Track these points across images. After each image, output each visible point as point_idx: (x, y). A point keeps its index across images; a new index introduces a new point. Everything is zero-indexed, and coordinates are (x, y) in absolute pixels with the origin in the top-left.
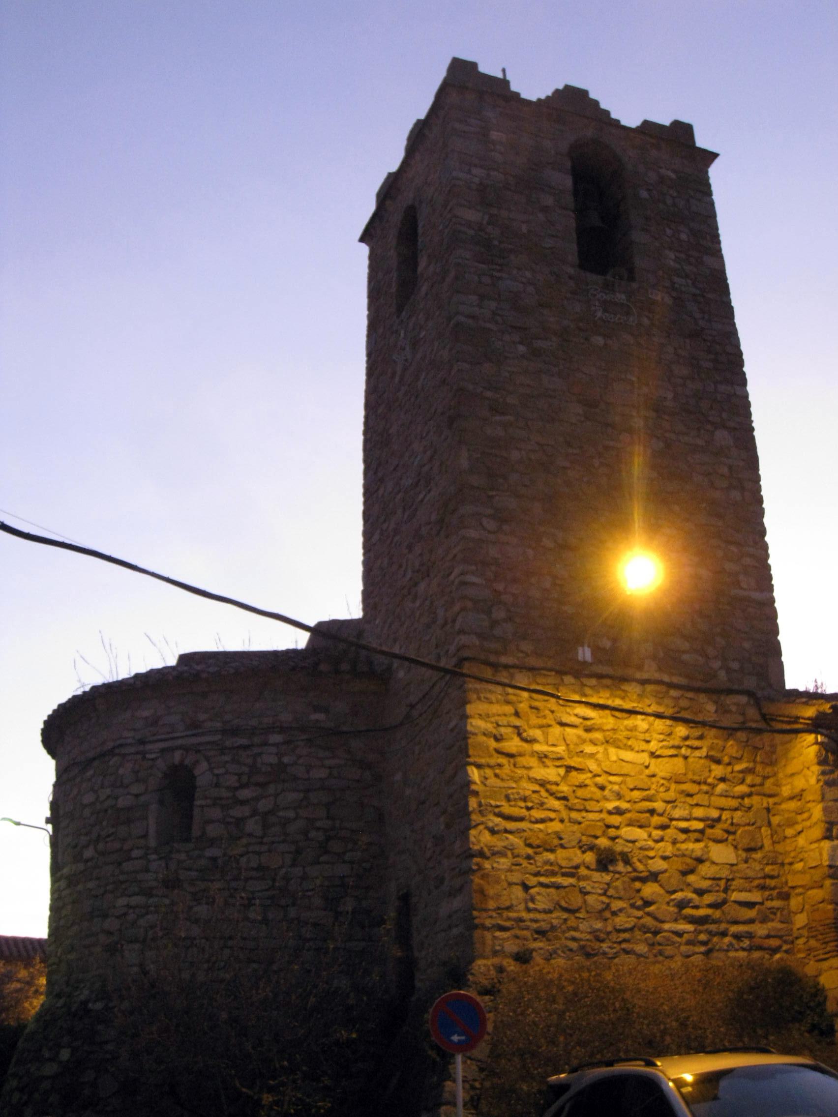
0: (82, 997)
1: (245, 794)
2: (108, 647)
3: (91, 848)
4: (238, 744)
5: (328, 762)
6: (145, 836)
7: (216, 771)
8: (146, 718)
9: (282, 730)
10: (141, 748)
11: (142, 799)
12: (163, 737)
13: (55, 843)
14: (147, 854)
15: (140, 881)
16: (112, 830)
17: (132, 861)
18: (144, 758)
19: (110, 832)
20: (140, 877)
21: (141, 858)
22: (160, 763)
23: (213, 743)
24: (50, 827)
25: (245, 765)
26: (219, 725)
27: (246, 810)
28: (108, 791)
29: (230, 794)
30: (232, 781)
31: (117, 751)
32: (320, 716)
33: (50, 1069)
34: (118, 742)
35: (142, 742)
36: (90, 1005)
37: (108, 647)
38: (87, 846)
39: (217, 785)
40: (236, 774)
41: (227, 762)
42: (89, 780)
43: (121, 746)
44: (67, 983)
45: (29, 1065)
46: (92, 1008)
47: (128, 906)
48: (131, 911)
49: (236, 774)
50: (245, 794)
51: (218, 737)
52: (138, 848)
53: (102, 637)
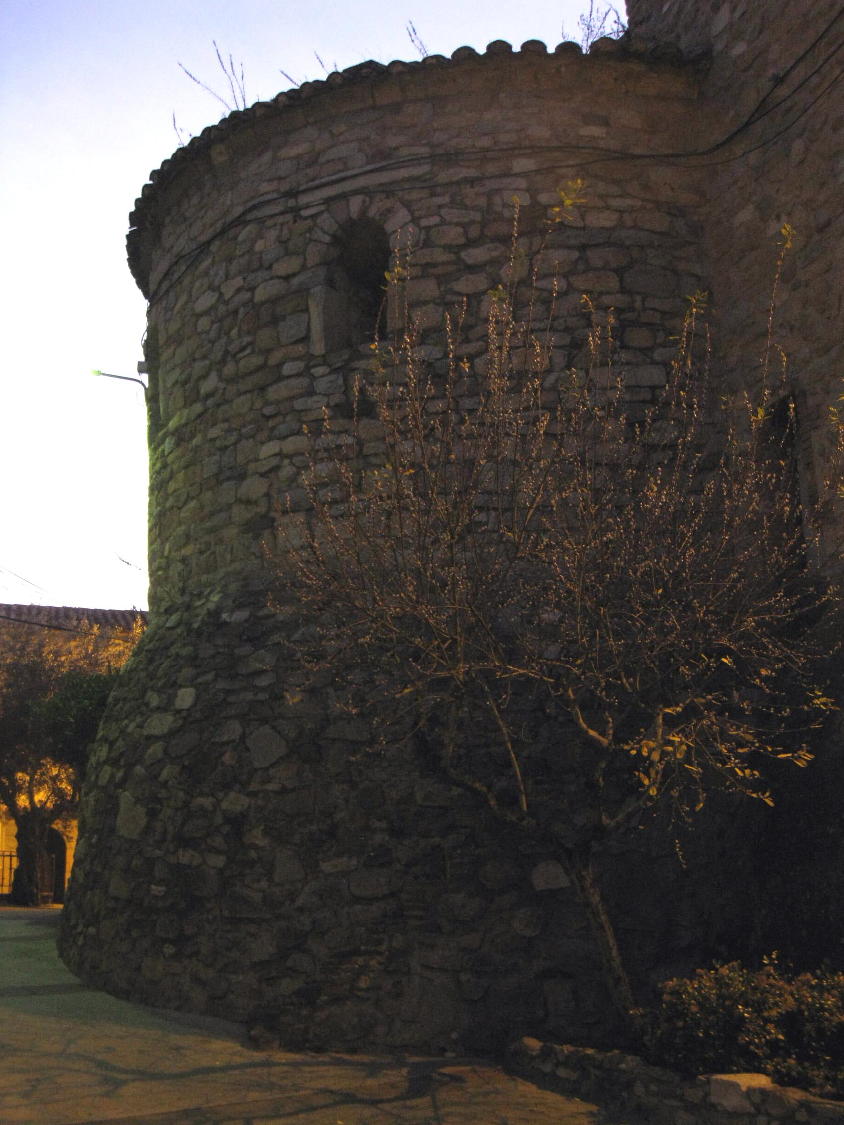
0: (211, 606)
1: (476, 255)
2: (227, 66)
3: (214, 376)
4: (461, 176)
5: (615, 203)
6: (305, 339)
7: (424, 223)
8: (299, 157)
9: (535, 150)
10: (291, 203)
11: (295, 281)
12: (326, 179)
13: (152, 397)
14: (308, 368)
15: (299, 412)
16: (247, 339)
17: (285, 382)
18: (297, 218)
19: (244, 343)
20: (299, 404)
21: (298, 375)
22: (327, 222)
23: (417, 179)
24: (145, 378)
25: (474, 208)
26: (424, 150)
27: (480, 282)
28: (238, 282)
29: (452, 257)
30: (453, 235)
31: (248, 217)
32: (597, 131)
33: (160, 724)
34: (250, 204)
35: (293, 194)
36: (225, 616)
37: (227, 66)
38: (204, 377)
39: (427, 243)
40: (457, 224)
41: (441, 207)
42: (206, 274)
43: (255, 207)
44: (183, 591)
45: (126, 722)
46: (228, 620)
47: (280, 454)
48: (286, 462)
49: (457, 224)
50: (476, 255)
51: (424, 169)
52: (294, 359)
53: (217, 50)
